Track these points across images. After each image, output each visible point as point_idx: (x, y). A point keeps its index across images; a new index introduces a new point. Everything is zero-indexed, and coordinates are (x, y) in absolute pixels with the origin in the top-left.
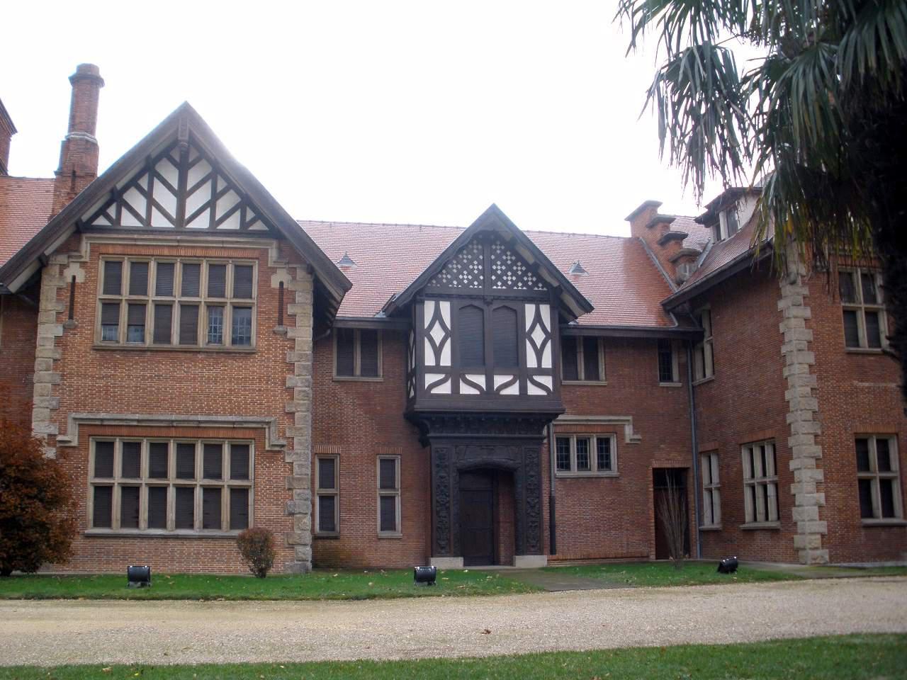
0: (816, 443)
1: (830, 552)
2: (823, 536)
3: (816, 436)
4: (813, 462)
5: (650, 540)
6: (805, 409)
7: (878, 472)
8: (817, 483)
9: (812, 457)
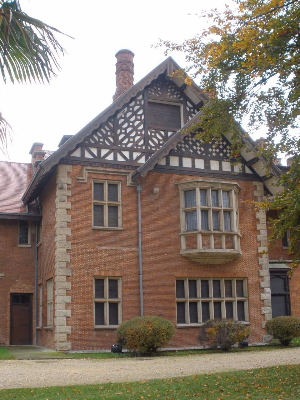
0: (68, 281)
1: (72, 344)
2: (68, 334)
3: (68, 277)
4: (65, 292)
5: (7, 334)
6: (62, 261)
7: (188, 298)
8: (66, 304)
9: (64, 289)
